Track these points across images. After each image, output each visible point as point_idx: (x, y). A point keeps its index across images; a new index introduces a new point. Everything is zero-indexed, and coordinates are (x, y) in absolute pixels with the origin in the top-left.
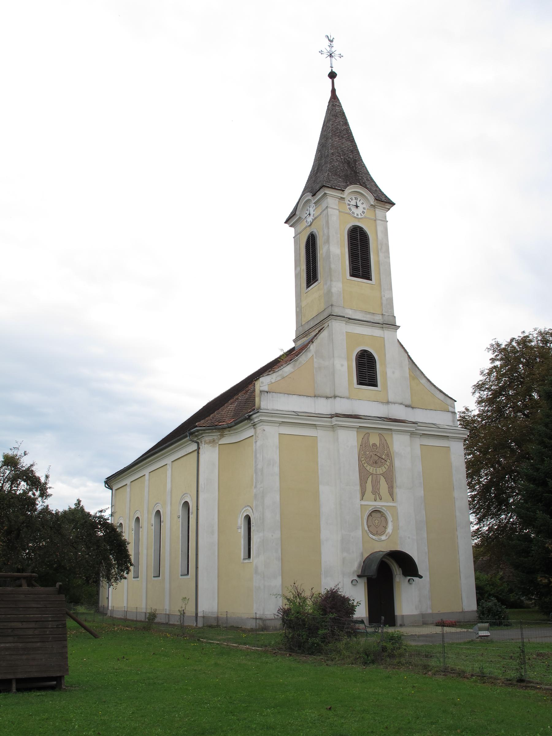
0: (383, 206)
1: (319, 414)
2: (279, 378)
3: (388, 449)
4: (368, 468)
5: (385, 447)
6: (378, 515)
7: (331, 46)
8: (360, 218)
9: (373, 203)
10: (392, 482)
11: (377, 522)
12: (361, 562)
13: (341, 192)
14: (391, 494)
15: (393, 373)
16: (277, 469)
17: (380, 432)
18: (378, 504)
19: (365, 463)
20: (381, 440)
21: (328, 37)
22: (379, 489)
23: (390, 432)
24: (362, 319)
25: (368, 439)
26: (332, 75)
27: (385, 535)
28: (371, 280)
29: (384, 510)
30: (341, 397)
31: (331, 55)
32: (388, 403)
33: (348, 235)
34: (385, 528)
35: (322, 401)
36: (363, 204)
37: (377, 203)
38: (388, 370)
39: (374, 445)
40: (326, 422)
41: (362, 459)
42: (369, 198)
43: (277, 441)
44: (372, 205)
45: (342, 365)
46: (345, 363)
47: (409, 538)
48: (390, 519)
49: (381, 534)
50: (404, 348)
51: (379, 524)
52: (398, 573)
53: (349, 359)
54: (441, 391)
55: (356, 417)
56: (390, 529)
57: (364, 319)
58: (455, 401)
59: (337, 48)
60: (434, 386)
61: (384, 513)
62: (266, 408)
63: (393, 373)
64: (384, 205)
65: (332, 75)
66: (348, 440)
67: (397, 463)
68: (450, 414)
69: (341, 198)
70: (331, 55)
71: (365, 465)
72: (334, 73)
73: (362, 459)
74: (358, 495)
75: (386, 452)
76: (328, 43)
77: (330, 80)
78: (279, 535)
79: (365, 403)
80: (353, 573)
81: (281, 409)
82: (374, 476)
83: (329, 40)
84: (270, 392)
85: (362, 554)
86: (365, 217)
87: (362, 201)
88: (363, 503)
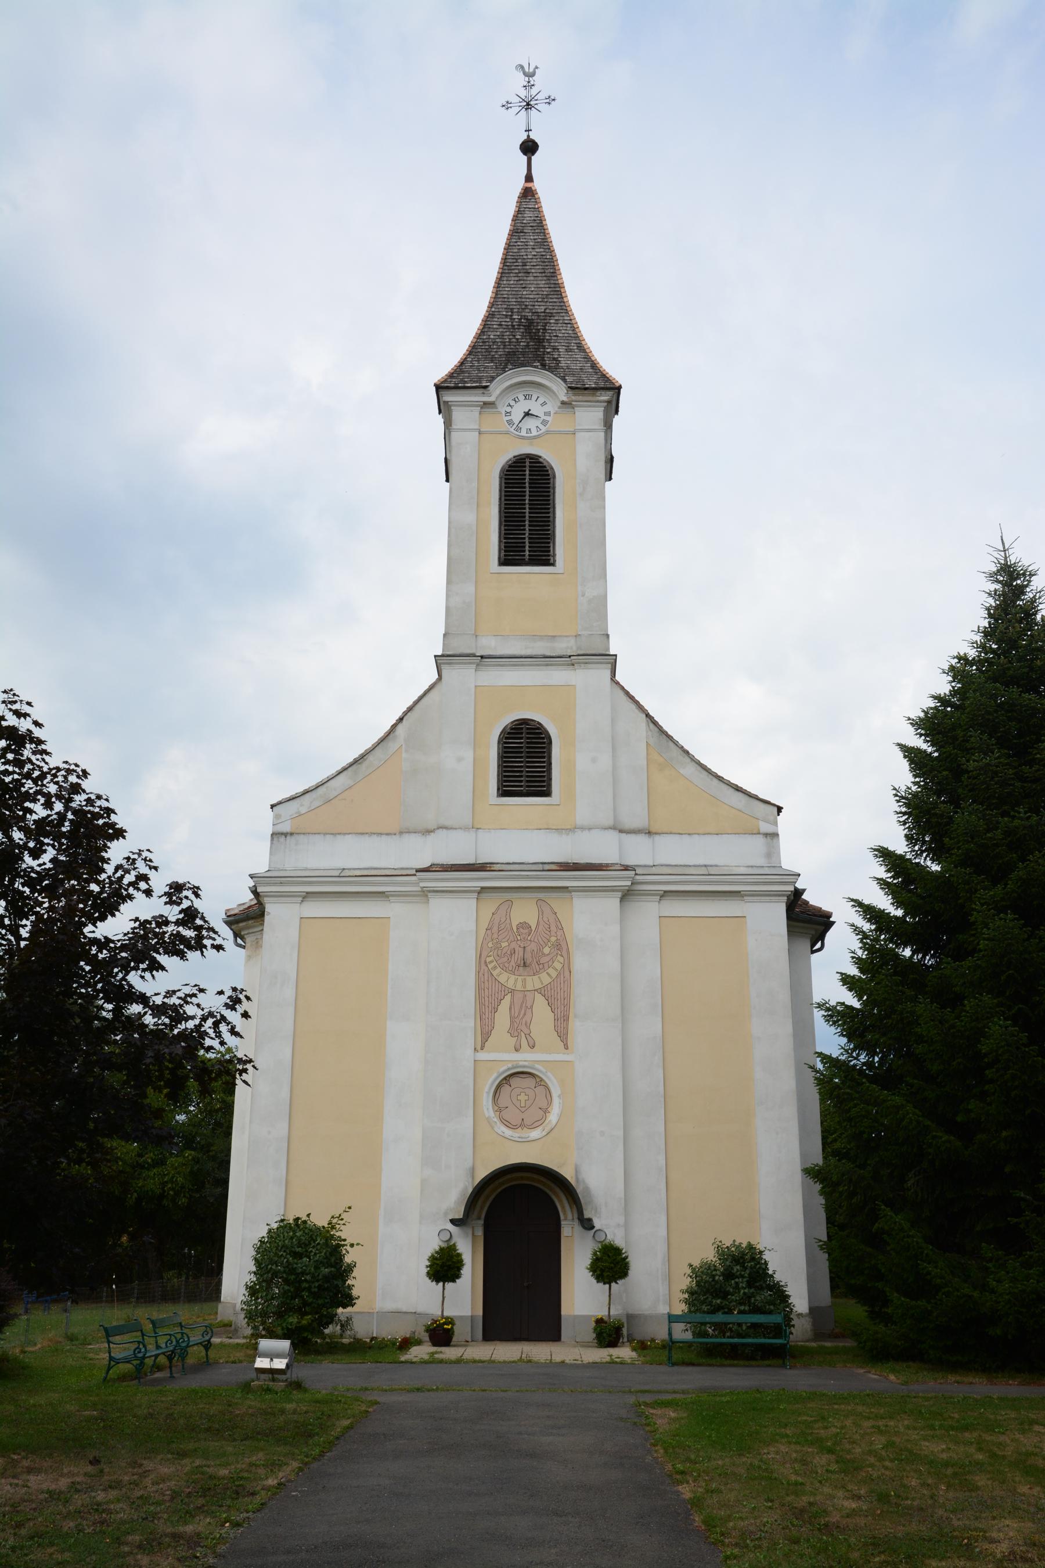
0: (590, 398)
1: (402, 869)
2: (317, 804)
3: (560, 933)
4: (503, 978)
5: (553, 928)
6: (529, 1082)
7: (529, 86)
8: (535, 437)
9: (565, 399)
10: (567, 1006)
11: (523, 1097)
12: (466, 1188)
13: (481, 391)
14: (563, 1036)
15: (594, 760)
16: (289, 992)
17: (541, 895)
18: (525, 1058)
19: (495, 968)
20: (541, 912)
21: (522, 67)
22: (528, 1025)
23: (567, 895)
24: (523, 653)
25: (508, 914)
26: (529, 148)
27: (541, 1128)
28: (553, 565)
29: (539, 1070)
30: (590, 829)
31: (528, 104)
32: (573, 829)
33: (501, 478)
34: (546, 1111)
35: (413, 841)
36: (544, 404)
37: (575, 395)
38: (577, 760)
39: (524, 925)
40: (411, 885)
41: (489, 960)
42: (554, 388)
43: (294, 933)
44: (563, 403)
45: (460, 759)
46: (469, 755)
47: (602, 1133)
48: (556, 1092)
49: (532, 1127)
50: (637, 703)
51: (529, 1103)
52: (570, 1216)
53: (476, 744)
54: (738, 789)
55: (482, 867)
56: (553, 1117)
57: (529, 652)
58: (779, 809)
59: (542, 85)
60: (720, 779)
61: (542, 1080)
62: (281, 867)
63: (594, 760)
64: (594, 395)
65: (529, 148)
66: (455, 923)
67: (579, 962)
68: (760, 840)
69: (485, 403)
70: (528, 104)
71: (495, 973)
72: (533, 142)
73: (489, 960)
74: (470, 1041)
75: (553, 939)
76: (522, 80)
77: (525, 158)
78: (285, 1132)
79: (521, 834)
80: (446, 1214)
81: (383, 866)
82: (519, 996)
83: (525, 74)
84: (292, 834)
85: (473, 1171)
86: (548, 432)
87: (541, 400)
88: (482, 1056)
